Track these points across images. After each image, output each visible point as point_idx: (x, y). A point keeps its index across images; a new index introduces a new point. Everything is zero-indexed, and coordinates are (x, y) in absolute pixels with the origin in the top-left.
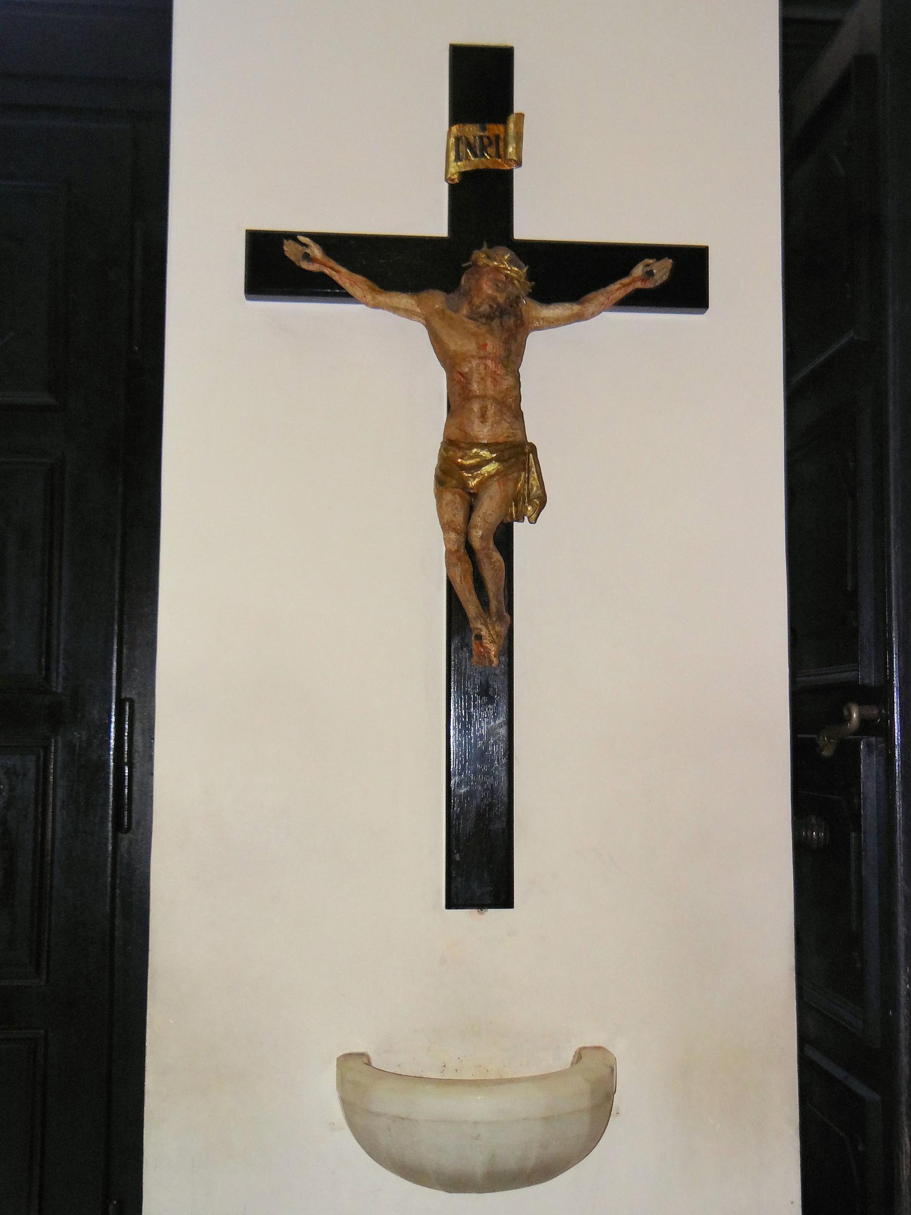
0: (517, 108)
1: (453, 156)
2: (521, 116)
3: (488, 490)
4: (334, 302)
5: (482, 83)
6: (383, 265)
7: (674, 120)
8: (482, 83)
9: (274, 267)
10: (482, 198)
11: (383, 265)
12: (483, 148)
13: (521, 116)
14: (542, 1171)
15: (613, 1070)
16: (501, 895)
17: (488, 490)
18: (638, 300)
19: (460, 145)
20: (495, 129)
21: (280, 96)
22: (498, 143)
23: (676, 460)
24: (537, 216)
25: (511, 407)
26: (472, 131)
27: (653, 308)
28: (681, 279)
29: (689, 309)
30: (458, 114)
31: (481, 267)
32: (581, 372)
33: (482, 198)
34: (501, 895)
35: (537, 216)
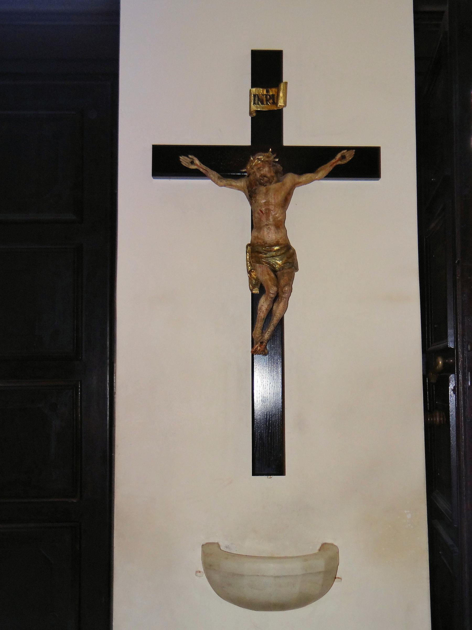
0: (284, 80)
1: (252, 103)
2: (286, 83)
3: (272, 270)
4: (165, 179)
5: (267, 68)
6: (221, 162)
7: (360, 88)
8: (267, 68)
9: (168, 162)
10: (267, 124)
11: (221, 162)
12: (267, 100)
13: (286, 83)
14: (303, 601)
15: (338, 553)
16: (279, 470)
17: (272, 270)
18: (337, 173)
19: (257, 99)
20: (272, 92)
21: (170, 84)
22: (274, 99)
23: (363, 250)
24: (295, 134)
25: (280, 225)
26: (262, 91)
27: (346, 178)
28: (364, 163)
29: (182, 177)
30: (256, 82)
31: (266, 160)
32: (317, 210)
33: (267, 124)
34: (279, 470)
35: (295, 134)
